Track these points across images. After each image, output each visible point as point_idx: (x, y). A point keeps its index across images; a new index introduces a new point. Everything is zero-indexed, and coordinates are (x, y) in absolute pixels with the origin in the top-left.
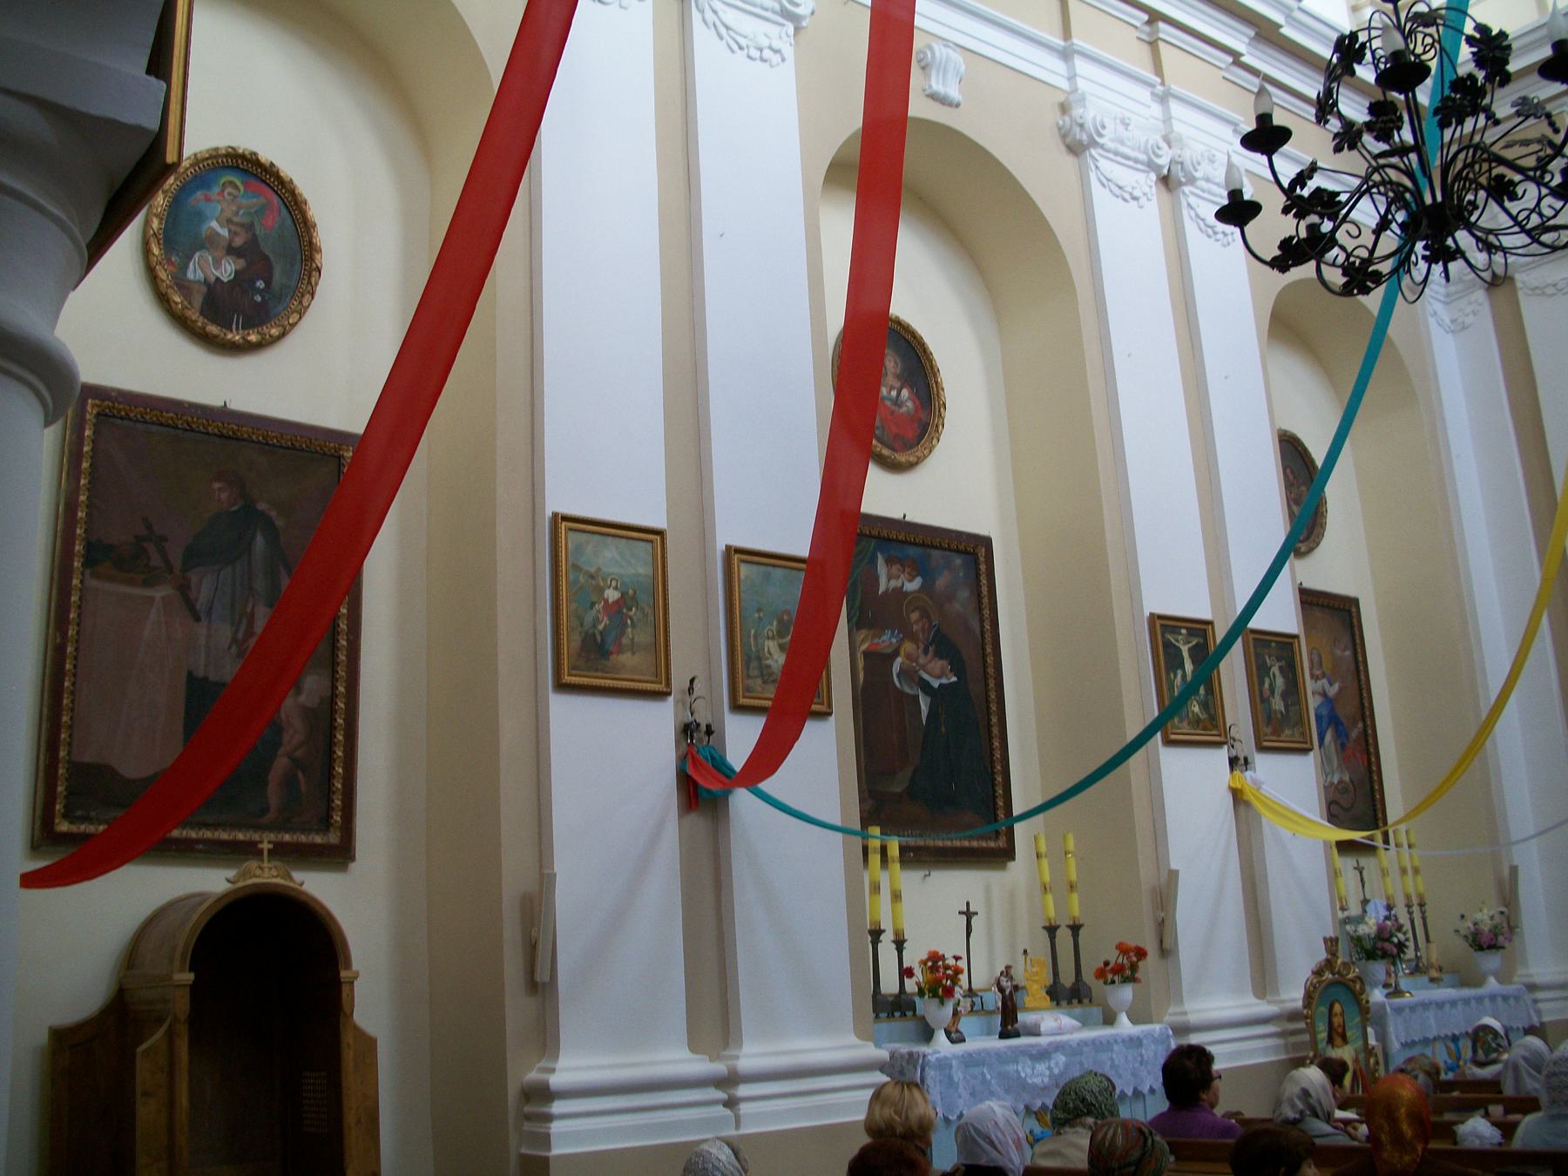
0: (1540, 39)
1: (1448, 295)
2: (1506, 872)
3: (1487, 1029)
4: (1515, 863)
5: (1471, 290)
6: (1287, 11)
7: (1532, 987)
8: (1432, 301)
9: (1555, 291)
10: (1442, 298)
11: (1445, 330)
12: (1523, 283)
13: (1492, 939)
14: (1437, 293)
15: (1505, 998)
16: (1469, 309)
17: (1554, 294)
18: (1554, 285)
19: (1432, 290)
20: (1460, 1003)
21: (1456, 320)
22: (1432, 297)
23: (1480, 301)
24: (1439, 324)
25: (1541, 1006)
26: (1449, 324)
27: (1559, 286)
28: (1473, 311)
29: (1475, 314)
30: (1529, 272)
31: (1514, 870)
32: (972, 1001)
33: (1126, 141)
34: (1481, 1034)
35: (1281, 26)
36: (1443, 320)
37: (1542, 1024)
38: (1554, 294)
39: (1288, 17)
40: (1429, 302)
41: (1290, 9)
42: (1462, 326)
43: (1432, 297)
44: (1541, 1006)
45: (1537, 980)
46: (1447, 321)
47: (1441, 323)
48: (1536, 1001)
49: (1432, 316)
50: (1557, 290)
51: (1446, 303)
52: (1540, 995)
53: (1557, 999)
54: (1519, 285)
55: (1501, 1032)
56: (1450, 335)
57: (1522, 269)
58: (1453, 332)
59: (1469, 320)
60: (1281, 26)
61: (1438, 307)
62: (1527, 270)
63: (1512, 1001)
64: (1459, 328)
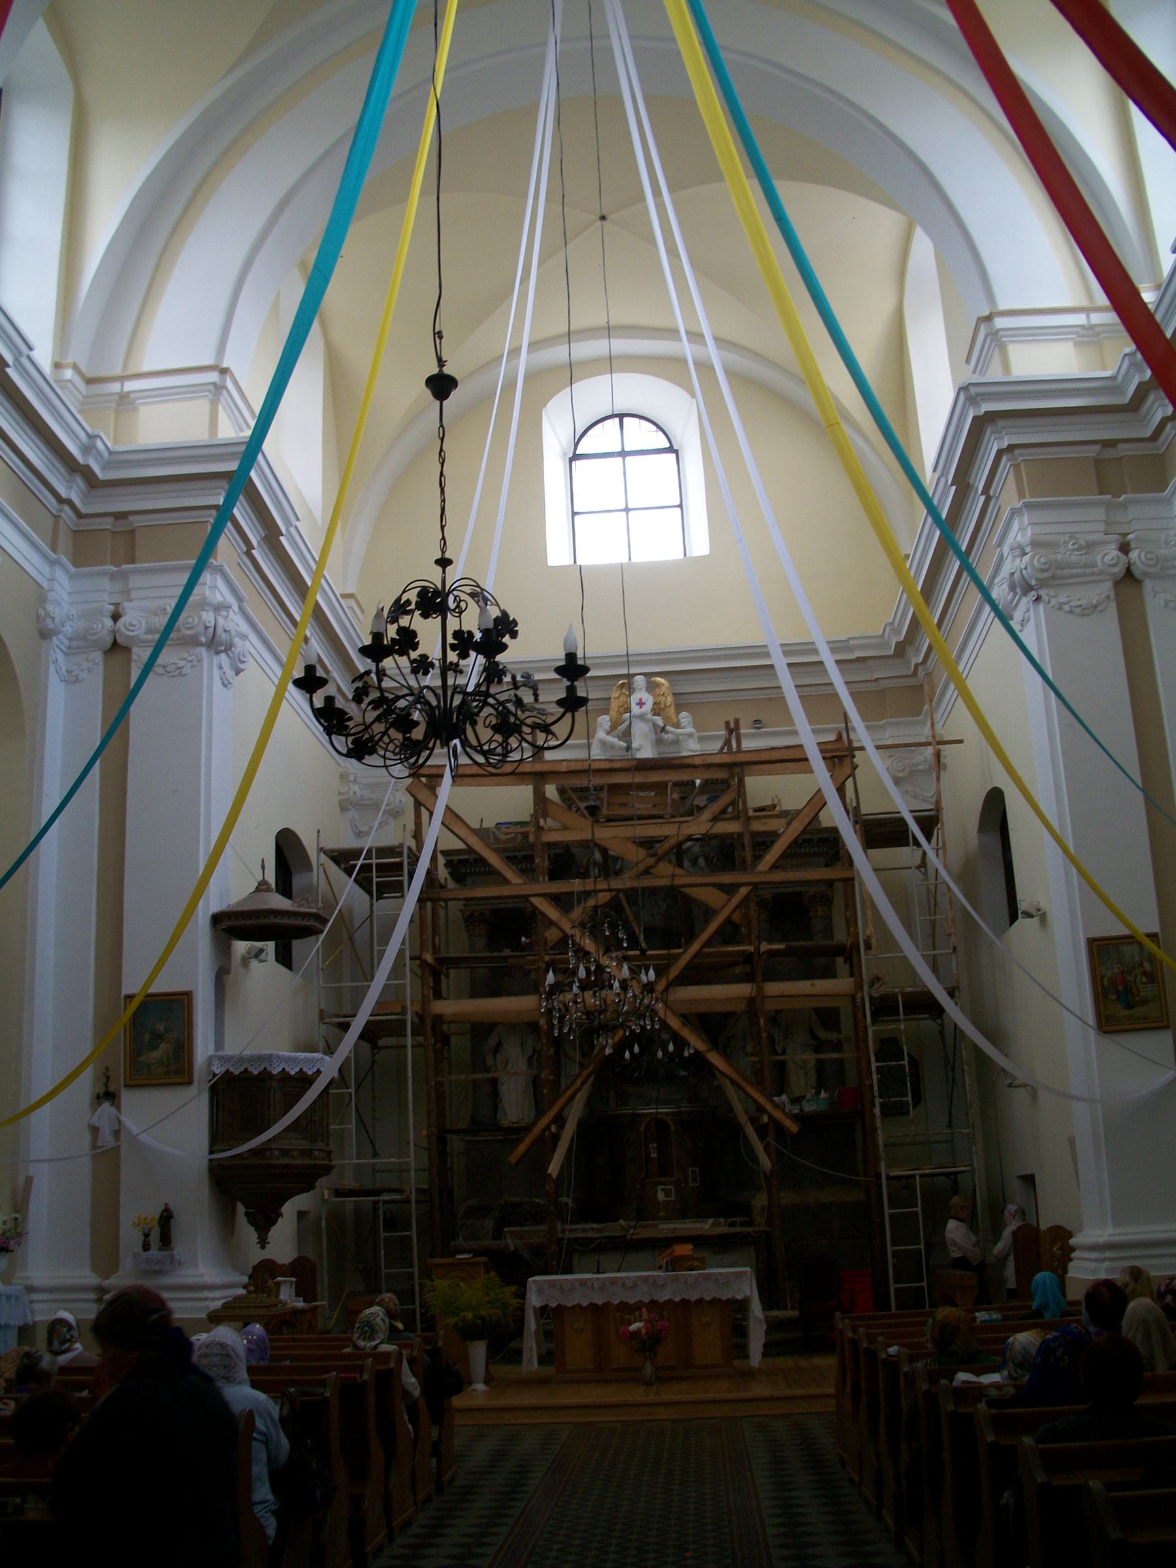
0: (234, 454)
1: (69, 648)
2: (21, 1182)
3: (62, 1322)
4: (31, 1174)
5: (91, 649)
6: (16, 353)
7: (30, 1289)
8: (56, 649)
9: (164, 672)
10: (63, 648)
11: (60, 677)
12: (139, 656)
13: (5, 1243)
14: (62, 643)
15: (9, 1297)
16: (85, 665)
17: (163, 674)
18: (165, 667)
19: (59, 640)
20: (14, 1298)
21: (72, 671)
22: (58, 647)
23: (97, 661)
24: (57, 672)
25: (35, 1306)
26: (65, 673)
27: (168, 669)
28: (88, 668)
29: (89, 671)
30: (146, 648)
31: (29, 1181)
32: (1024, 1220)
33: (1012, 571)
34: (58, 1327)
35: (8, 366)
36: (61, 669)
37: (35, 1323)
38: (163, 674)
39: (17, 360)
40: (54, 650)
41: (20, 353)
42: (75, 678)
43: (58, 647)
44: (35, 1306)
45: (35, 1282)
46: (64, 670)
47: (59, 670)
48: (31, 1302)
49: (53, 662)
50: (166, 671)
51: (65, 654)
52: (36, 1296)
53: (53, 1301)
54: (134, 657)
55: (74, 1324)
56: (63, 684)
57: (140, 645)
58: (66, 681)
59: (84, 675)
60: (8, 366)
61: (60, 657)
62: (145, 646)
63: (13, 1301)
64: (72, 680)
